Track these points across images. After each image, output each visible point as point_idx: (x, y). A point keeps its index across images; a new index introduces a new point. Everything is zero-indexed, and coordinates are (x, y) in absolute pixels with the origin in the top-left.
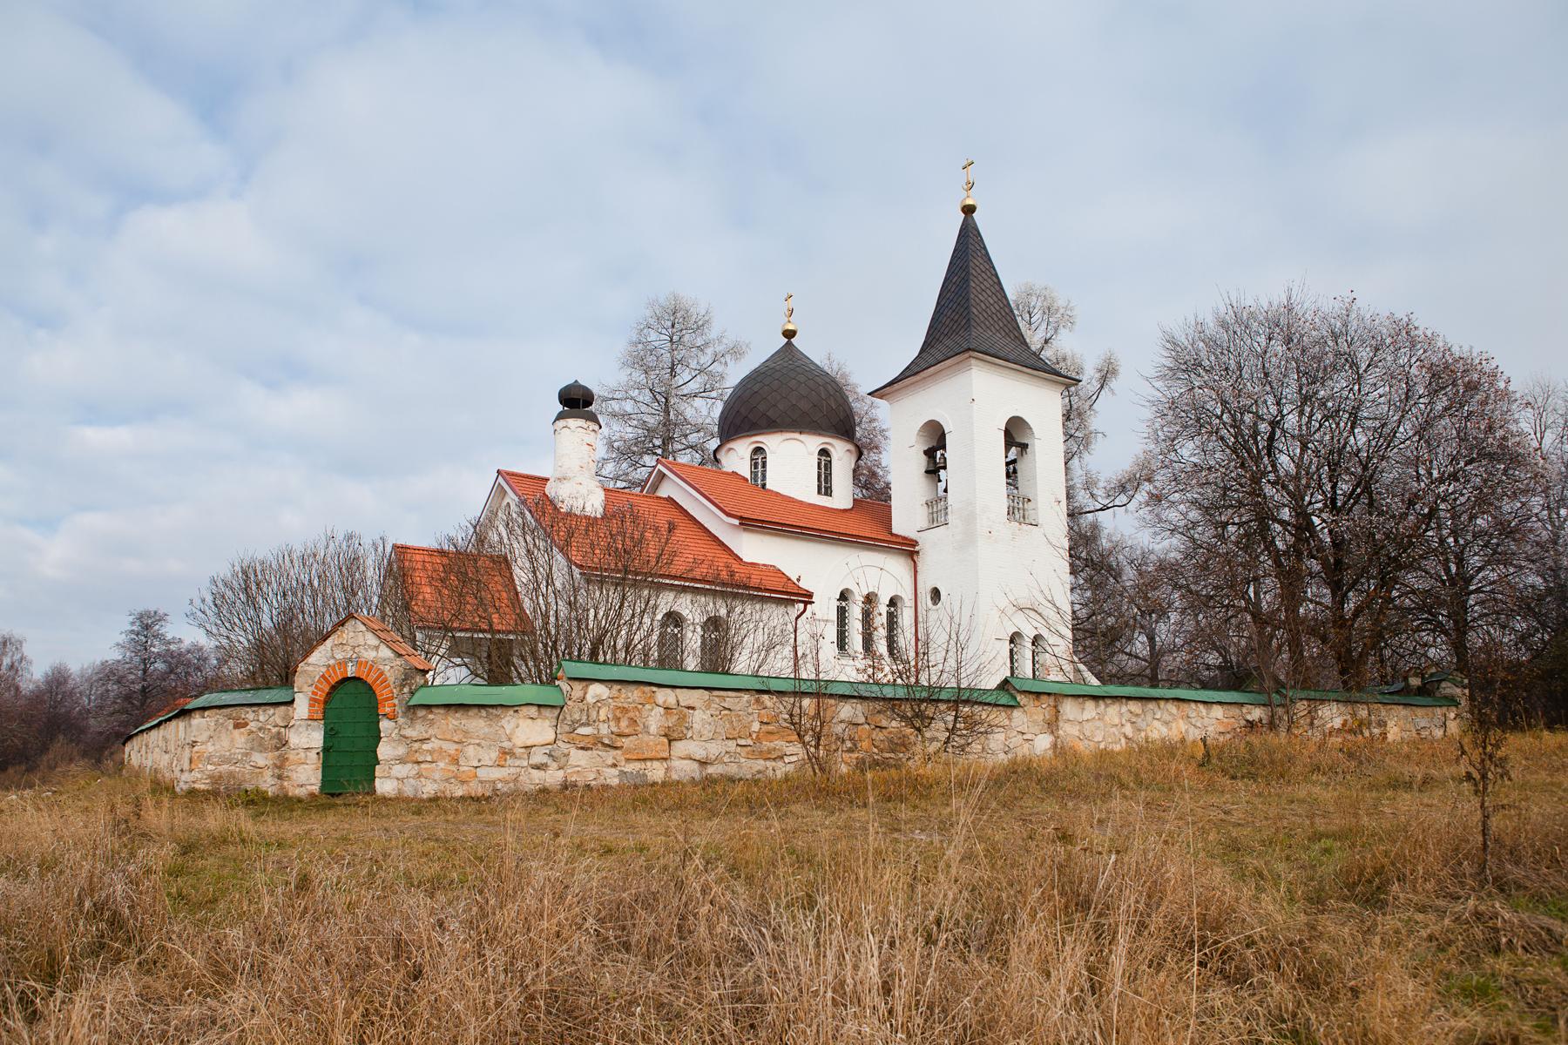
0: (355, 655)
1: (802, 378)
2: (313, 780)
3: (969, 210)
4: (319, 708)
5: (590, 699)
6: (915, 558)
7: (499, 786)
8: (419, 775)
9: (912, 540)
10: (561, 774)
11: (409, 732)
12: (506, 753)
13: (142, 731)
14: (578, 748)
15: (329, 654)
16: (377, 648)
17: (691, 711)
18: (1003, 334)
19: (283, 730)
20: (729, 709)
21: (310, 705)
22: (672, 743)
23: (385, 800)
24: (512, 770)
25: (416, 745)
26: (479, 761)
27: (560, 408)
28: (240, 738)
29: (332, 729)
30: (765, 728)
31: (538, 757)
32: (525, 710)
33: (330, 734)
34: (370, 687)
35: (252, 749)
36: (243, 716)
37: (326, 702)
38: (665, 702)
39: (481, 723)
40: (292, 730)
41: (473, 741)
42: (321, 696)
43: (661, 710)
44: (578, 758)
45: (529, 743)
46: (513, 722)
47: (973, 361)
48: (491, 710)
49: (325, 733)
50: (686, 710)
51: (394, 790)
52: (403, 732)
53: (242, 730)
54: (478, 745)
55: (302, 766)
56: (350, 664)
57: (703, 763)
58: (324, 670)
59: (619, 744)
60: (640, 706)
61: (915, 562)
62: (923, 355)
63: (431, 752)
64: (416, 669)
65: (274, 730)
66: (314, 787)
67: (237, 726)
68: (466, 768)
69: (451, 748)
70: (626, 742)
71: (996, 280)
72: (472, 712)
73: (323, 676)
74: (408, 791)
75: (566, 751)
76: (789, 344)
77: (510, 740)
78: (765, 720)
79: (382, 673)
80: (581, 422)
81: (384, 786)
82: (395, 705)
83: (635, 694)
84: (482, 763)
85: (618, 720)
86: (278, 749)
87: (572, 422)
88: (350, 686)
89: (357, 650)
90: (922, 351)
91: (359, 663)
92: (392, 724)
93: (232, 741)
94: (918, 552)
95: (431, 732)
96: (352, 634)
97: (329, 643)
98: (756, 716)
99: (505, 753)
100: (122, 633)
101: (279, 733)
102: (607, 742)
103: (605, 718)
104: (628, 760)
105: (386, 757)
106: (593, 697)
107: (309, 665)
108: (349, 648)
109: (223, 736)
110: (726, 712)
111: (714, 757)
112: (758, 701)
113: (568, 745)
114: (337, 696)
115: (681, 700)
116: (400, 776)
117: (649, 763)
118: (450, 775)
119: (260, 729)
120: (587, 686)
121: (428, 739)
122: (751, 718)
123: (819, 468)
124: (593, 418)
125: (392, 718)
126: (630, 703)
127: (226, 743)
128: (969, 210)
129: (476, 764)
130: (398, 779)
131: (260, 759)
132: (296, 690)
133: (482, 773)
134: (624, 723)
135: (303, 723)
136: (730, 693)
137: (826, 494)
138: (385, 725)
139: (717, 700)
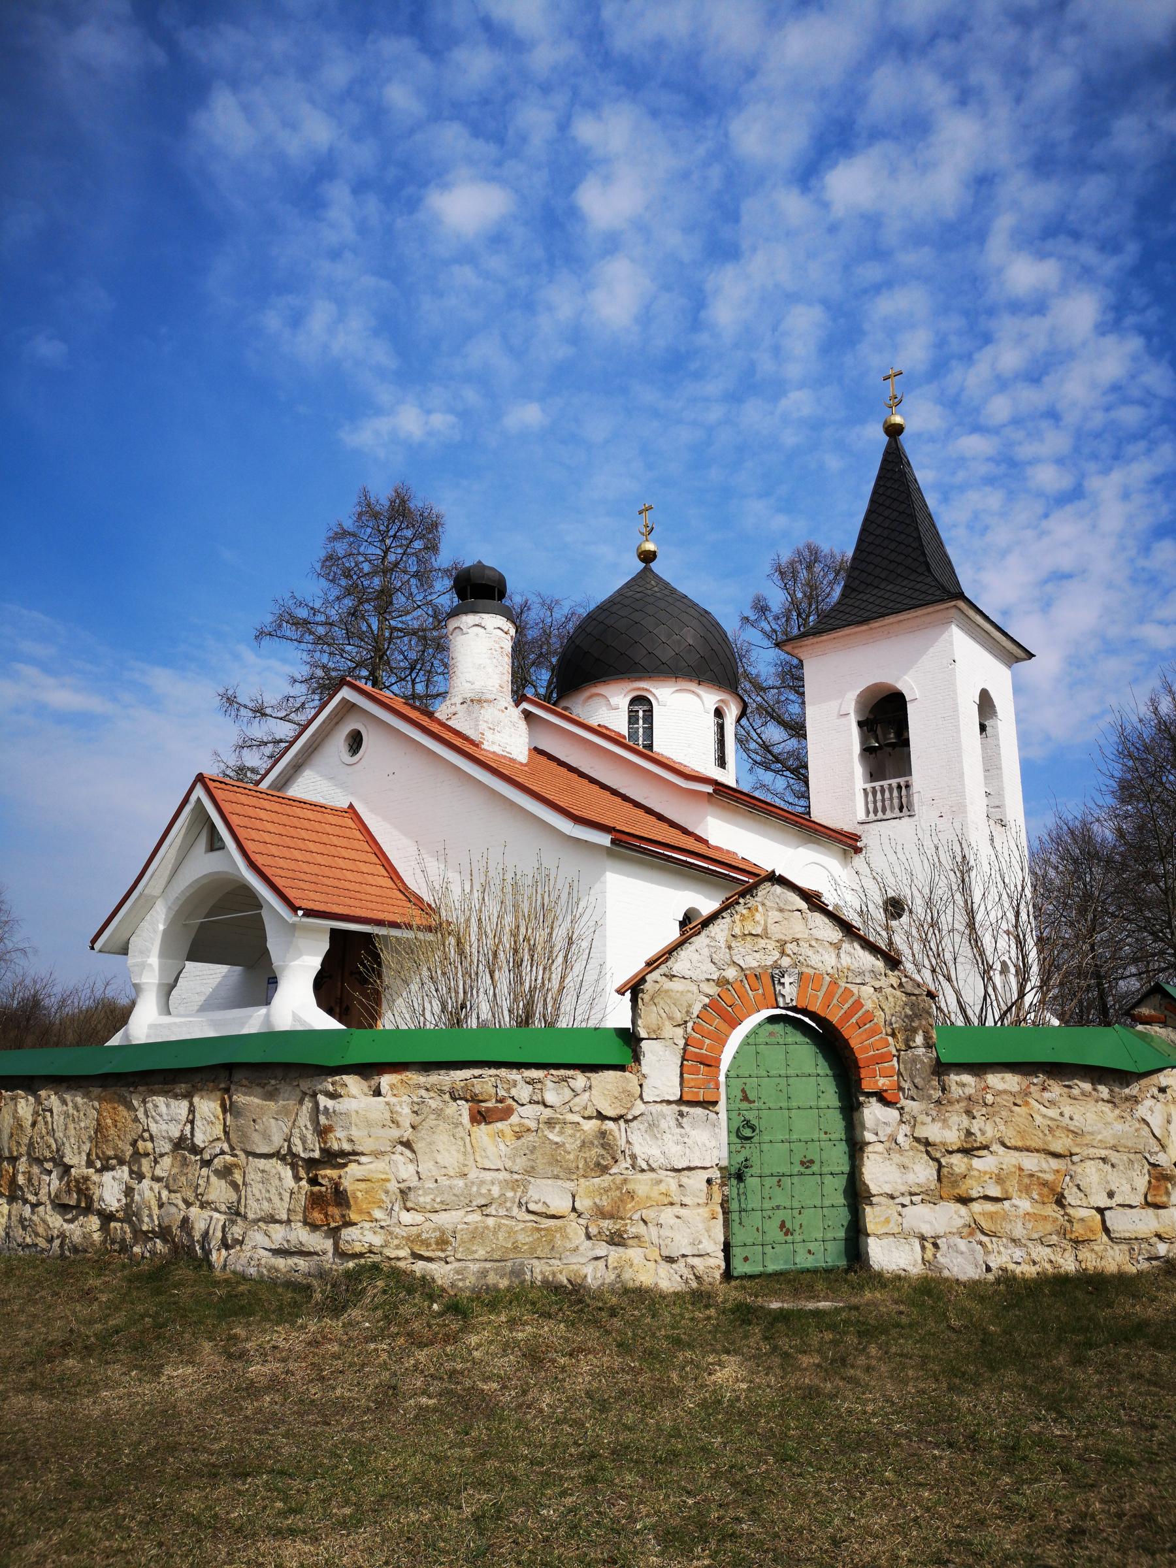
3: (894, 431)
9: (856, 835)
26: (1111, 1195)
35: (530, 1171)
47: (953, 611)
53: (499, 1125)
67: (481, 1117)
76: (647, 570)
79: (858, 1004)
84: (1118, 1199)
92: (892, 1114)
96: (774, 915)
109: (442, 1139)
129: (1103, 1202)
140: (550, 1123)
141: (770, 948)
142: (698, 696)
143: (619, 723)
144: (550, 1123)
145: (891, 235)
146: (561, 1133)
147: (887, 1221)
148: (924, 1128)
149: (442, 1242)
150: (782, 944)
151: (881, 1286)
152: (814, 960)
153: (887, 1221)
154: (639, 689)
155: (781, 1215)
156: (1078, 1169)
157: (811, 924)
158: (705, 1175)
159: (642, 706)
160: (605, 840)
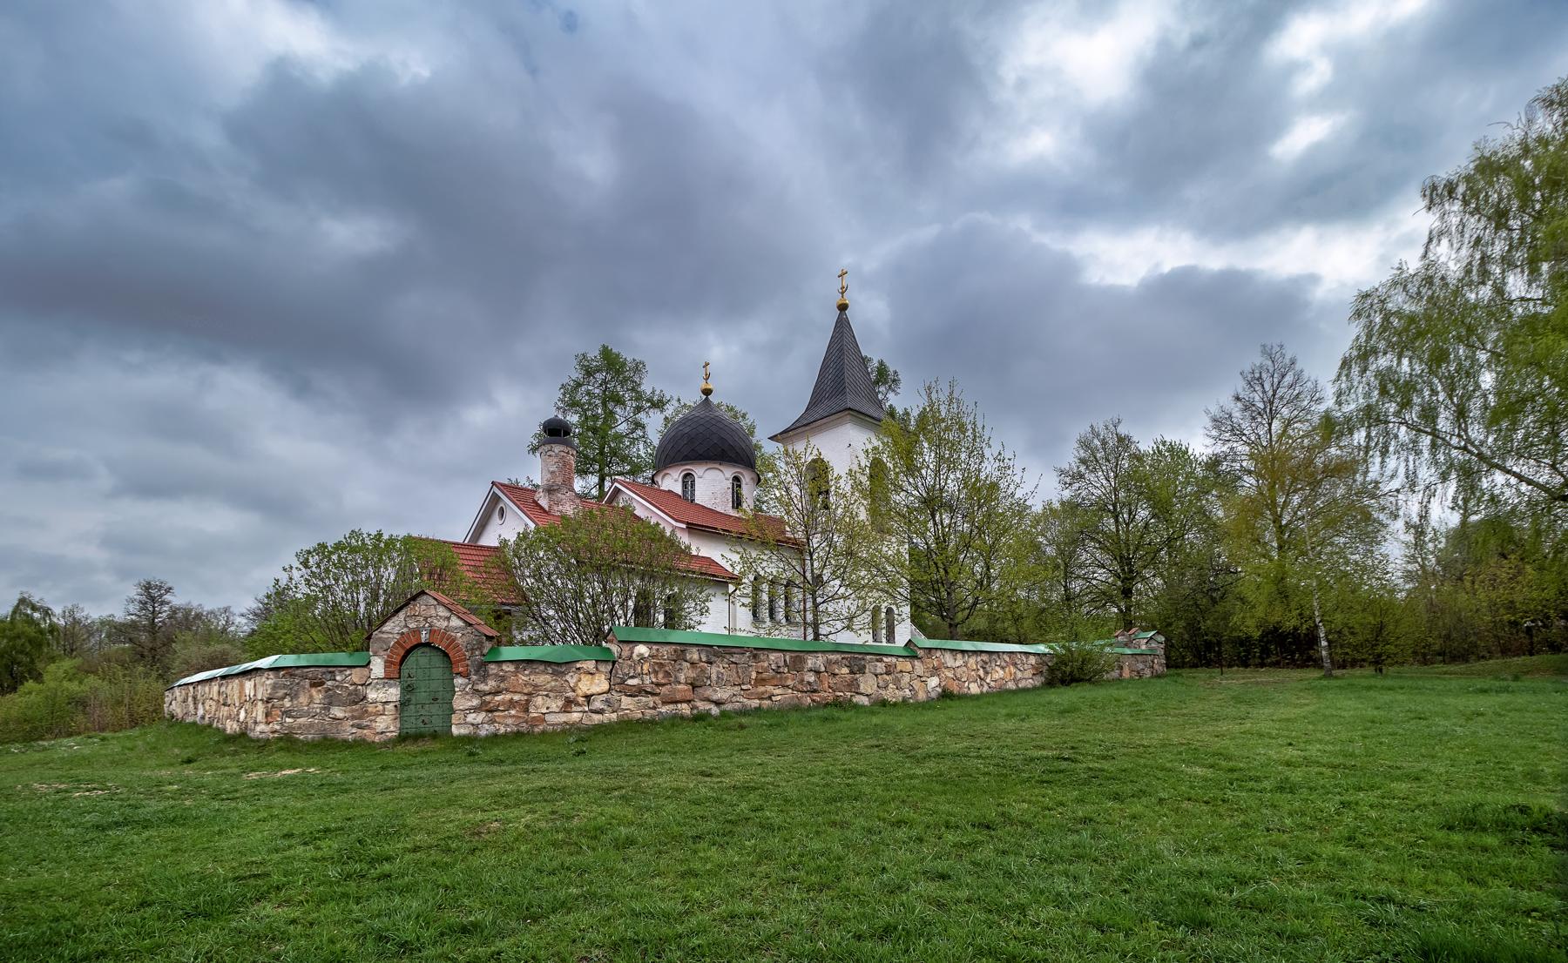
2: (392, 728)
4: (394, 668)
11: (482, 687)
21: (386, 667)
25: (488, 698)
30: (760, 676)
35: (330, 704)
37: (401, 663)
42: (397, 659)
44: (626, 702)
45: (589, 693)
54: (547, 696)
59: (658, 691)
64: (486, 636)
70: (664, 690)
76: (707, 399)
77: (574, 691)
91: (432, 632)
96: (423, 607)
99: (572, 702)
101: (356, 690)
104: (664, 703)
114: (411, 659)
116: (475, 722)
117: (679, 705)
120: (633, 647)
128: (843, 308)
129: (544, 711)
130: (473, 725)
133: (551, 719)
134: (660, 675)
135: (380, 681)
140: (337, 687)
143: (678, 489)
145: (1360, 307)
149: (299, 728)
151: (1443, 473)
152: (438, 624)
155: (423, 718)
158: (392, 704)
159: (688, 481)
160: (684, 526)
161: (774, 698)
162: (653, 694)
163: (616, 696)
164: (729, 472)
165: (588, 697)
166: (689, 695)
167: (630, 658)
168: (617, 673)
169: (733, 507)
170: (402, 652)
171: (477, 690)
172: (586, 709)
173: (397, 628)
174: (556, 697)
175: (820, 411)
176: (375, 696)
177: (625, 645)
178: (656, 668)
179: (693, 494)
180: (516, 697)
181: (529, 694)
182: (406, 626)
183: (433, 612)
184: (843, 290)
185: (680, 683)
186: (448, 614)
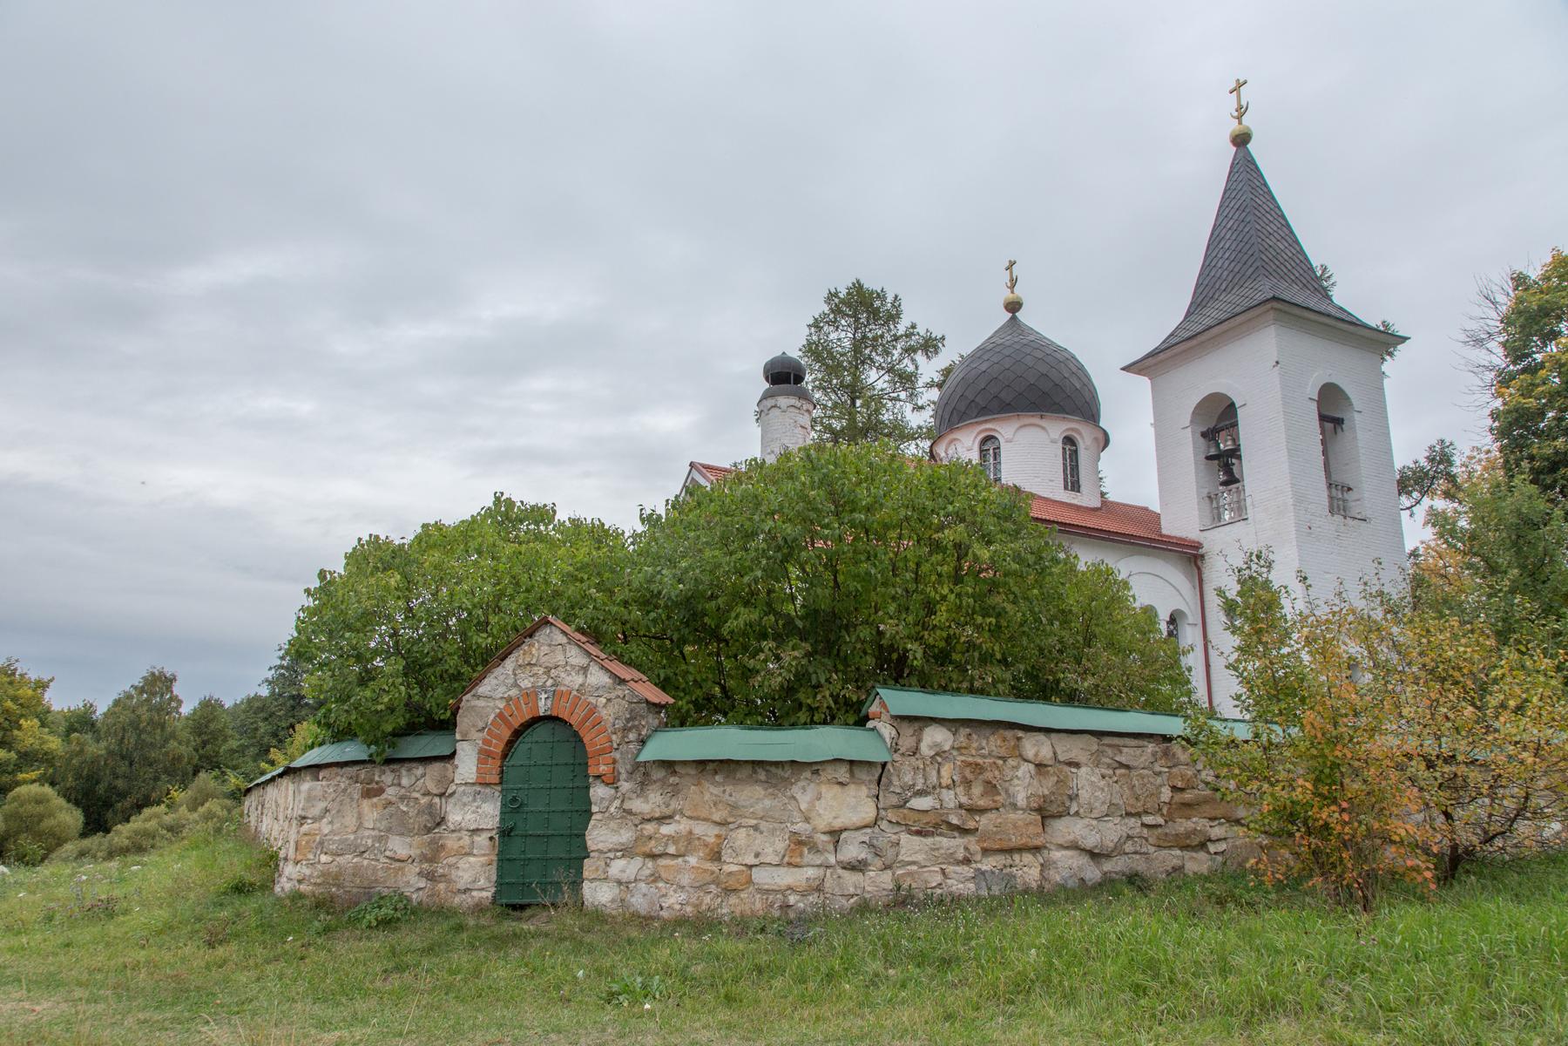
0: (550, 682)
1: (1039, 354)
2: (482, 883)
4: (493, 766)
5: (925, 749)
6: (1199, 563)
7: (792, 899)
8: (655, 878)
10: (886, 879)
11: (638, 805)
12: (800, 842)
13: (258, 785)
14: (911, 833)
15: (511, 681)
16: (584, 670)
17: (1074, 770)
18: (1301, 285)
19: (437, 800)
20: (1127, 767)
21: (480, 761)
22: (1047, 823)
23: (599, 917)
24: (811, 872)
25: (649, 828)
26: (757, 855)
27: (767, 385)
28: (371, 813)
29: (514, 800)
30: (1179, 797)
31: (852, 850)
32: (829, 772)
33: (512, 808)
34: (576, 734)
35: (389, 830)
36: (377, 778)
37: (505, 756)
38: (1036, 755)
39: (759, 791)
40: (452, 800)
41: (745, 821)
42: (498, 748)
43: (1031, 767)
44: (912, 848)
45: (837, 824)
46: (812, 789)
48: (773, 769)
49: (503, 805)
50: (1066, 768)
51: (613, 901)
52: (627, 806)
53: (375, 800)
54: (756, 828)
55: (466, 858)
56: (544, 696)
57: (1094, 855)
58: (501, 705)
59: (971, 825)
60: (1000, 762)
61: (1199, 569)
62: (1193, 318)
63: (672, 839)
64: (647, 702)
65: (424, 801)
66: (485, 894)
68: (734, 868)
69: (707, 832)
70: (984, 822)
71: (1284, 223)
72: (744, 773)
73: (500, 715)
74: (639, 902)
75: (894, 837)
76: (1014, 318)
77: (807, 820)
78: (1179, 785)
80: (793, 401)
81: (598, 894)
82: (614, 762)
83: (993, 744)
84: (762, 859)
85: (967, 783)
86: (429, 830)
87: (783, 401)
88: (541, 732)
89: (553, 673)
90: (1188, 314)
91: (556, 695)
93: (360, 816)
94: (1202, 556)
95: (674, 805)
96: (545, 649)
97: (509, 664)
98: (1165, 776)
99: (800, 843)
100: (270, 669)
101: (431, 805)
102: (955, 821)
103: (950, 781)
104: (986, 852)
105: (600, 846)
106: (931, 748)
107: (479, 697)
108: (541, 671)
110: (1123, 771)
111: (1111, 845)
112: (1166, 753)
113: (897, 829)
114: (522, 747)
115: (1059, 752)
116: (624, 878)
117: (1017, 857)
118: (708, 878)
119: (402, 798)
120: (921, 729)
121: (670, 817)
122: (1159, 780)
123: (1064, 459)
124: (804, 396)
125: (612, 781)
126: (984, 757)
127: (350, 821)
128: (1241, 140)
129: (750, 860)
130: (619, 883)
131: (400, 846)
132: (458, 737)
133: (762, 877)
134: (977, 790)
135: (469, 789)
136: (1128, 741)
137: (1072, 490)
138: (599, 792)
139: (1109, 751)
141: (540, 672)
142: (1043, 428)
144: (402, 798)
146: (407, 805)
147: (597, 870)
148: (630, 802)
150: (548, 670)
153: (597, 870)
154: (987, 430)
156: (733, 834)
157: (568, 655)
158: (487, 835)
159: (989, 445)
161: (1212, 848)
162: (963, 831)
163: (889, 833)
164: (1056, 429)
165: (835, 834)
166: (1032, 834)
167: (915, 752)
168: (891, 782)
169: (1066, 488)
170: (506, 734)
171: (630, 812)
172: (832, 860)
173: (502, 689)
174: (773, 832)
175: (1213, 314)
176: (459, 818)
177: (905, 724)
178: (970, 776)
179: (997, 470)
180: (700, 829)
181: (723, 824)
182: (516, 685)
183: (559, 658)
184: (1241, 111)
185: (1014, 806)
186: (583, 661)
